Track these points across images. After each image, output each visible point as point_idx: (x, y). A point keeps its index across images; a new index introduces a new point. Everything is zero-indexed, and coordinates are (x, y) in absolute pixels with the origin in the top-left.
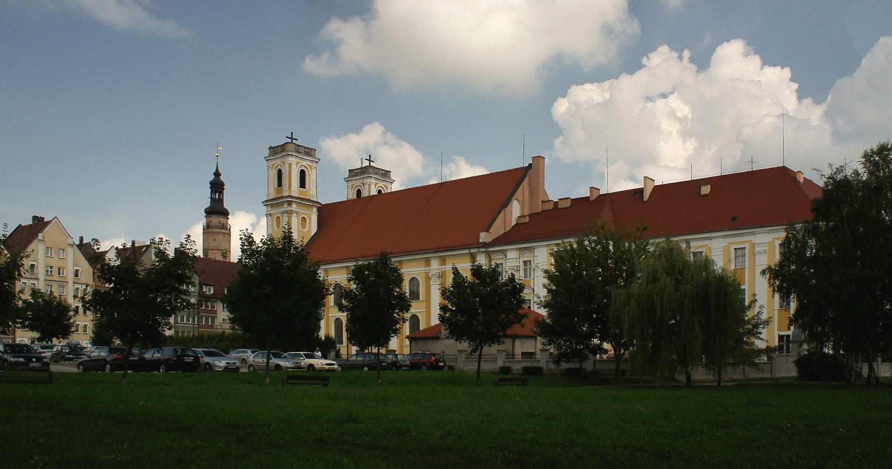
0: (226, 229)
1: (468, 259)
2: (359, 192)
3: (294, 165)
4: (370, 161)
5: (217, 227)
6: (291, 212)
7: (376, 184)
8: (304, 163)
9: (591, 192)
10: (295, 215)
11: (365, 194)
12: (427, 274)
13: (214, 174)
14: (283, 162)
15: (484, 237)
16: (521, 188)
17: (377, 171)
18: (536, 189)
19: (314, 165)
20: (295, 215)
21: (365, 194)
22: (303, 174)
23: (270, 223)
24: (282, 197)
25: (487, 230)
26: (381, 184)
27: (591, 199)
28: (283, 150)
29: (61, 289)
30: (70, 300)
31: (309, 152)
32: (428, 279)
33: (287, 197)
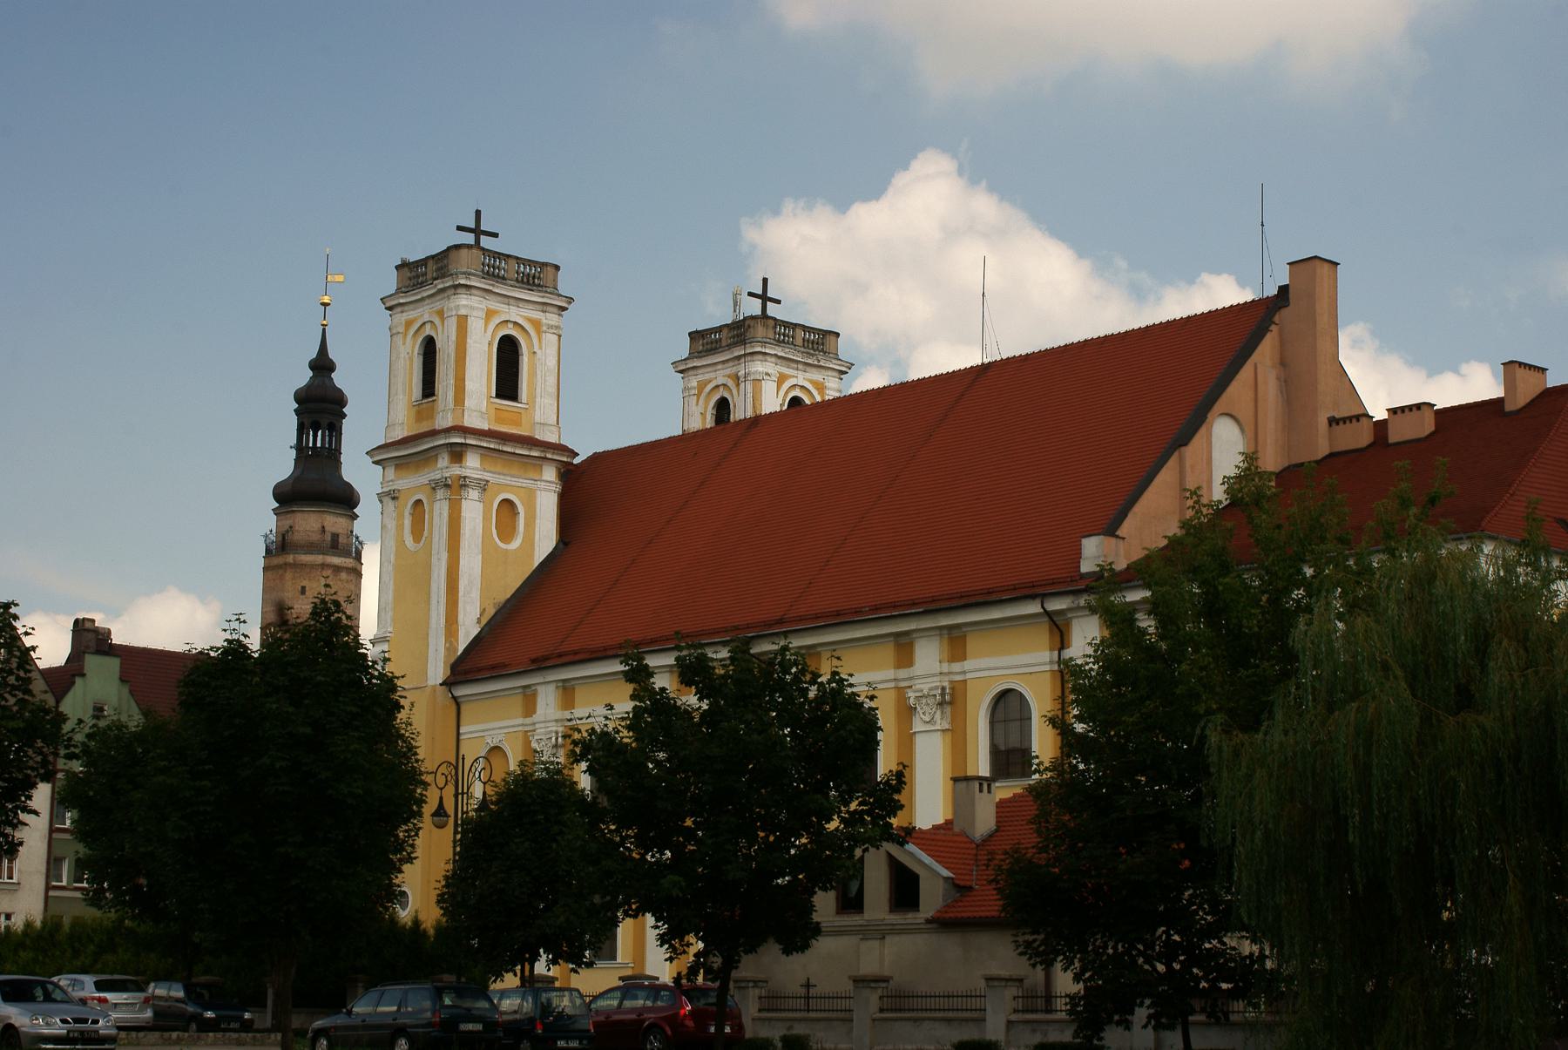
0: (347, 554)
1: (1042, 635)
2: (723, 406)
3: (476, 321)
4: (764, 298)
5: (311, 548)
6: (463, 484)
7: (781, 379)
8: (515, 314)
9: (1509, 383)
10: (474, 494)
11: (739, 412)
12: (901, 692)
13: (314, 365)
14: (441, 313)
15: (1093, 552)
16: (1246, 373)
17: (786, 333)
18: (1311, 375)
19: (551, 318)
20: (474, 494)
21: (739, 412)
22: (508, 352)
23: (391, 525)
24: (434, 433)
25: (1111, 530)
26: (802, 378)
27: (1509, 407)
28: (443, 273)
29: (836, 662)
30: (968, 665)
31: (535, 276)
32: (906, 712)
33: (448, 431)
